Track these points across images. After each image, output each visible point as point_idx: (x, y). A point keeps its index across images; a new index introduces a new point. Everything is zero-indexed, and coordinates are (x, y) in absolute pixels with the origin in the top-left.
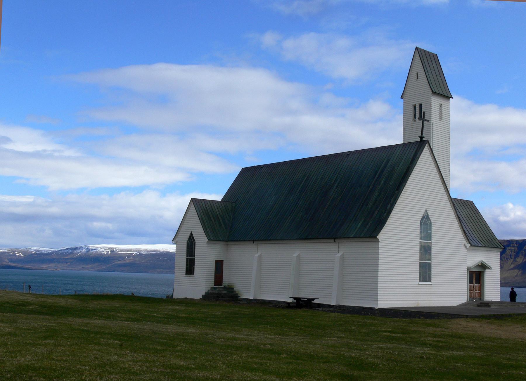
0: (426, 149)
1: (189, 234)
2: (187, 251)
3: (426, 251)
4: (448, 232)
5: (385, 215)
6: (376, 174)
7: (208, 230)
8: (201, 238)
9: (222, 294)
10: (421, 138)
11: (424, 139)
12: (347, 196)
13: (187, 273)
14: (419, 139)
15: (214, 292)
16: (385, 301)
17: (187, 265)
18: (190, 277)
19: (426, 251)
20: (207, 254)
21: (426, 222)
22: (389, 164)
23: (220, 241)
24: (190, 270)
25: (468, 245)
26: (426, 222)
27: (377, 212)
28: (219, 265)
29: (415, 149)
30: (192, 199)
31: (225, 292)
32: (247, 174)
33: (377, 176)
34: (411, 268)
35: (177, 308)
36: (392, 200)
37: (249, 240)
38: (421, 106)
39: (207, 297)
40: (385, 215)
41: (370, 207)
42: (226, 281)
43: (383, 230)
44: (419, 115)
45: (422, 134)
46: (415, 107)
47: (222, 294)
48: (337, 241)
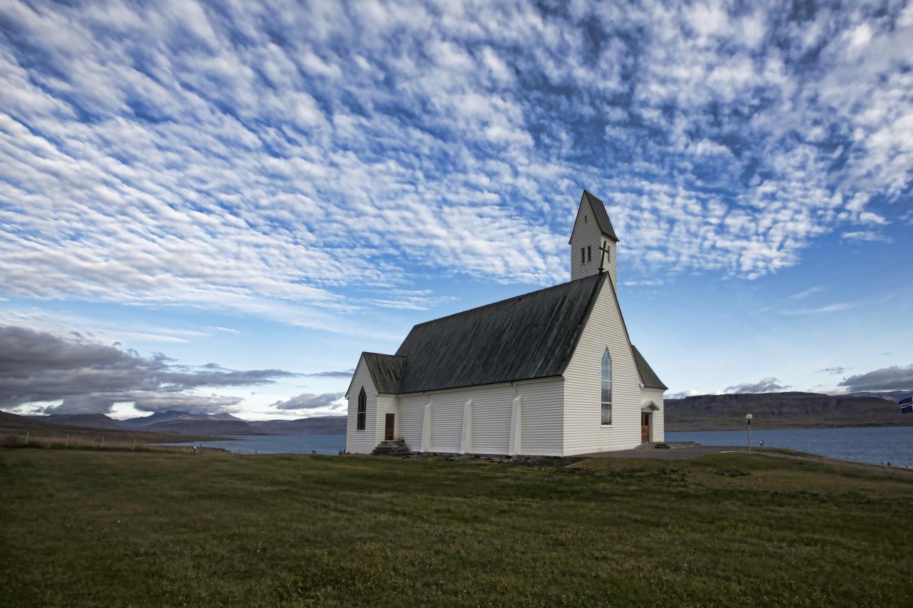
0: (607, 282)
1: (360, 389)
2: (359, 405)
3: (606, 396)
4: (625, 374)
5: (569, 350)
6: (552, 312)
7: (379, 383)
8: (371, 391)
9: (394, 450)
10: (601, 269)
11: (604, 271)
12: (526, 339)
13: (358, 429)
14: (598, 272)
15: (384, 446)
16: (569, 451)
17: (358, 420)
18: (361, 433)
19: (606, 396)
20: (381, 406)
21: (607, 360)
22: (566, 301)
23: (391, 393)
24: (361, 425)
25: (642, 385)
26: (607, 360)
27: (558, 349)
28: (390, 419)
29: (595, 282)
30: (363, 353)
31: (396, 446)
32: (416, 328)
33: (554, 314)
34: (588, 418)
35: (342, 466)
36: (575, 335)
37: (419, 392)
38: (589, 248)
39: (378, 451)
40: (569, 350)
41: (550, 345)
42: (397, 434)
43: (568, 367)
44: (583, 254)
45: (602, 265)
46: (583, 250)
47: (394, 450)
48: (514, 384)
